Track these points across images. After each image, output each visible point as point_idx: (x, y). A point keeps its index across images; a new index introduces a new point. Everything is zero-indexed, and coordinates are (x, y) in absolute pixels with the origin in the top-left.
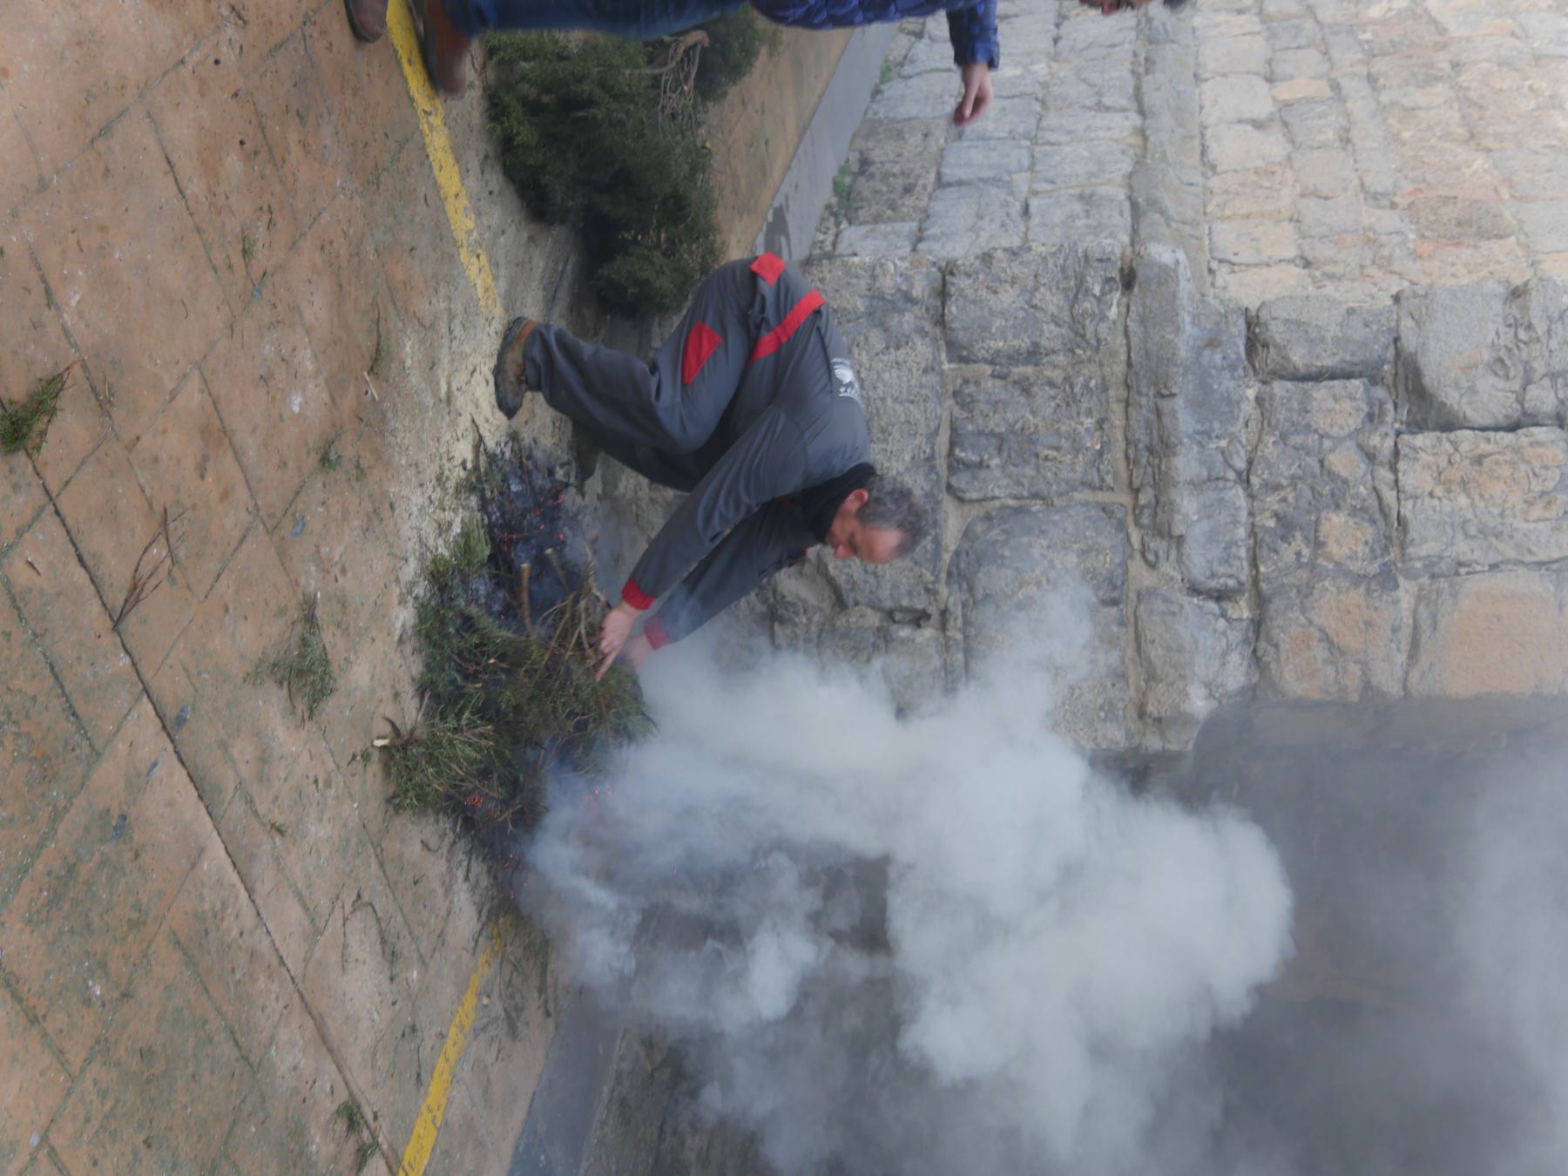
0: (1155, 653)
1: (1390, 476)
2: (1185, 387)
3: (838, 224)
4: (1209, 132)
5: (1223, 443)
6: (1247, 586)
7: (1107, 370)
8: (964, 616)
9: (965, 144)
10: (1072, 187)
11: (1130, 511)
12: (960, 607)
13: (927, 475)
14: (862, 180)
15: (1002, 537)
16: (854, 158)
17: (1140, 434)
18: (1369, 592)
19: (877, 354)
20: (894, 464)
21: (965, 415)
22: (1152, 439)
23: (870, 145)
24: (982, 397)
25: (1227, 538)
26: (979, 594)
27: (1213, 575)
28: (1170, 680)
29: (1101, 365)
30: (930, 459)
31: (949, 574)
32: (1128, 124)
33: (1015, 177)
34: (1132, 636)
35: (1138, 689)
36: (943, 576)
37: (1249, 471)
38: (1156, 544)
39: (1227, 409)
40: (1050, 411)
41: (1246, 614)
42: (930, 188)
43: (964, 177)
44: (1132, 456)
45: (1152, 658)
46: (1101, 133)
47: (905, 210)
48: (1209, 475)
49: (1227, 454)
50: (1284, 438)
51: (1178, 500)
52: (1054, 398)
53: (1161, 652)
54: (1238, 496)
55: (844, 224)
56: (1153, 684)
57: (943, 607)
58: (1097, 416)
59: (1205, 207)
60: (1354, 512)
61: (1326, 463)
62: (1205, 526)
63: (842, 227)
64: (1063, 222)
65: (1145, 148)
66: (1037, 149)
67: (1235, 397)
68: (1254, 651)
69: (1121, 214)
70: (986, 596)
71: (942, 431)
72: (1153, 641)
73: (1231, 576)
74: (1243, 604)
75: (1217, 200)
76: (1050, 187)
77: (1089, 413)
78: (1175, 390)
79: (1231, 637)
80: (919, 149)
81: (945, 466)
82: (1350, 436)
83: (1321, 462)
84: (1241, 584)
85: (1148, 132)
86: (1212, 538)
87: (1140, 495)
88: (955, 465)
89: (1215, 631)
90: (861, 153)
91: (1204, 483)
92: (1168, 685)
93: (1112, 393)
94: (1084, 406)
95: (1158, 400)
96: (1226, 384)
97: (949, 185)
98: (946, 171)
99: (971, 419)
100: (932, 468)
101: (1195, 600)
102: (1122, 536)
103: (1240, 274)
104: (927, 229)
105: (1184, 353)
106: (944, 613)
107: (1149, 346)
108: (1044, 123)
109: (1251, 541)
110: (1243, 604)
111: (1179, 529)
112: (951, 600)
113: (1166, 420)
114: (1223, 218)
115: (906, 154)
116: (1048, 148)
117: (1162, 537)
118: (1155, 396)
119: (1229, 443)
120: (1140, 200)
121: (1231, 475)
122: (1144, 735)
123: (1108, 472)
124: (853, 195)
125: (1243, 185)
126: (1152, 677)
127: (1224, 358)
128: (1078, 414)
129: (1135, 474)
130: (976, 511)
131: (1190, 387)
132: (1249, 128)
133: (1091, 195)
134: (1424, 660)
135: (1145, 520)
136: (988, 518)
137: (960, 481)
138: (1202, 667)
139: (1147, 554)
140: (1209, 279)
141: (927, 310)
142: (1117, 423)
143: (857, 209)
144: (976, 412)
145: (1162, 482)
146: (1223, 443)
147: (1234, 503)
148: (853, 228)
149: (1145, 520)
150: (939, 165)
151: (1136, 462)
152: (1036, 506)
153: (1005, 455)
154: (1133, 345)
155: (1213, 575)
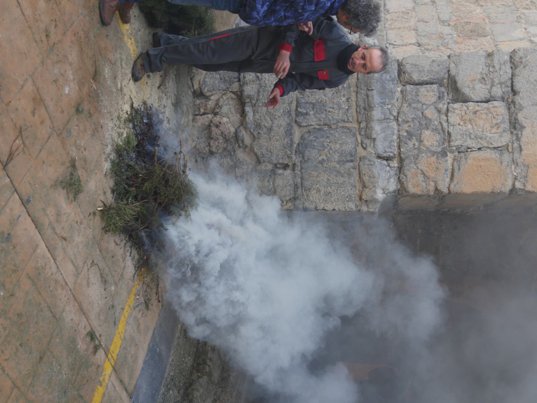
0: (366, 178)
1: (446, 118)
5: (389, 106)
6: (397, 156)
8: (301, 166)
11: (358, 130)
13: (288, 117)
18: (437, 158)
21: (301, 96)
22: (365, 105)
25: (390, 139)
26: (306, 159)
27: (385, 152)
28: (370, 188)
30: (289, 111)
31: (296, 151)
35: (359, 190)
36: (294, 152)
37: (398, 116)
38: (367, 141)
40: (330, 95)
41: (396, 165)
44: (358, 111)
48: (385, 118)
49: (391, 110)
50: (410, 105)
51: (374, 126)
53: (367, 178)
54: (394, 124)
56: (365, 189)
58: (346, 97)
59: (385, 25)
60: (433, 130)
61: (424, 113)
62: (383, 135)
68: (399, 178)
72: (365, 174)
73: (391, 152)
74: (395, 161)
75: (389, 22)
77: (344, 96)
78: (373, 88)
81: (294, 114)
82: (432, 104)
83: (422, 113)
84: (395, 155)
86: (385, 139)
87: (361, 124)
88: (298, 114)
89: (386, 171)
92: (370, 189)
93: (352, 89)
94: (342, 93)
95: (367, 91)
99: (303, 98)
100: (290, 114)
101: (379, 160)
103: (396, 49)
106: (294, 165)
109: (398, 140)
111: (374, 136)
112: (297, 160)
113: (370, 98)
114: (391, 29)
117: (368, 139)
121: (392, 118)
122: (361, 206)
123: (350, 117)
125: (398, 17)
126: (364, 186)
127: (390, 77)
129: (359, 117)
130: (305, 130)
131: (379, 87)
134: (455, 180)
135: (363, 133)
136: (309, 132)
137: (300, 119)
138: (381, 183)
139: (363, 145)
142: (353, 99)
144: (305, 95)
145: (368, 120)
146: (389, 106)
149: (363, 133)
151: (360, 113)
152: (326, 128)
155: (385, 152)
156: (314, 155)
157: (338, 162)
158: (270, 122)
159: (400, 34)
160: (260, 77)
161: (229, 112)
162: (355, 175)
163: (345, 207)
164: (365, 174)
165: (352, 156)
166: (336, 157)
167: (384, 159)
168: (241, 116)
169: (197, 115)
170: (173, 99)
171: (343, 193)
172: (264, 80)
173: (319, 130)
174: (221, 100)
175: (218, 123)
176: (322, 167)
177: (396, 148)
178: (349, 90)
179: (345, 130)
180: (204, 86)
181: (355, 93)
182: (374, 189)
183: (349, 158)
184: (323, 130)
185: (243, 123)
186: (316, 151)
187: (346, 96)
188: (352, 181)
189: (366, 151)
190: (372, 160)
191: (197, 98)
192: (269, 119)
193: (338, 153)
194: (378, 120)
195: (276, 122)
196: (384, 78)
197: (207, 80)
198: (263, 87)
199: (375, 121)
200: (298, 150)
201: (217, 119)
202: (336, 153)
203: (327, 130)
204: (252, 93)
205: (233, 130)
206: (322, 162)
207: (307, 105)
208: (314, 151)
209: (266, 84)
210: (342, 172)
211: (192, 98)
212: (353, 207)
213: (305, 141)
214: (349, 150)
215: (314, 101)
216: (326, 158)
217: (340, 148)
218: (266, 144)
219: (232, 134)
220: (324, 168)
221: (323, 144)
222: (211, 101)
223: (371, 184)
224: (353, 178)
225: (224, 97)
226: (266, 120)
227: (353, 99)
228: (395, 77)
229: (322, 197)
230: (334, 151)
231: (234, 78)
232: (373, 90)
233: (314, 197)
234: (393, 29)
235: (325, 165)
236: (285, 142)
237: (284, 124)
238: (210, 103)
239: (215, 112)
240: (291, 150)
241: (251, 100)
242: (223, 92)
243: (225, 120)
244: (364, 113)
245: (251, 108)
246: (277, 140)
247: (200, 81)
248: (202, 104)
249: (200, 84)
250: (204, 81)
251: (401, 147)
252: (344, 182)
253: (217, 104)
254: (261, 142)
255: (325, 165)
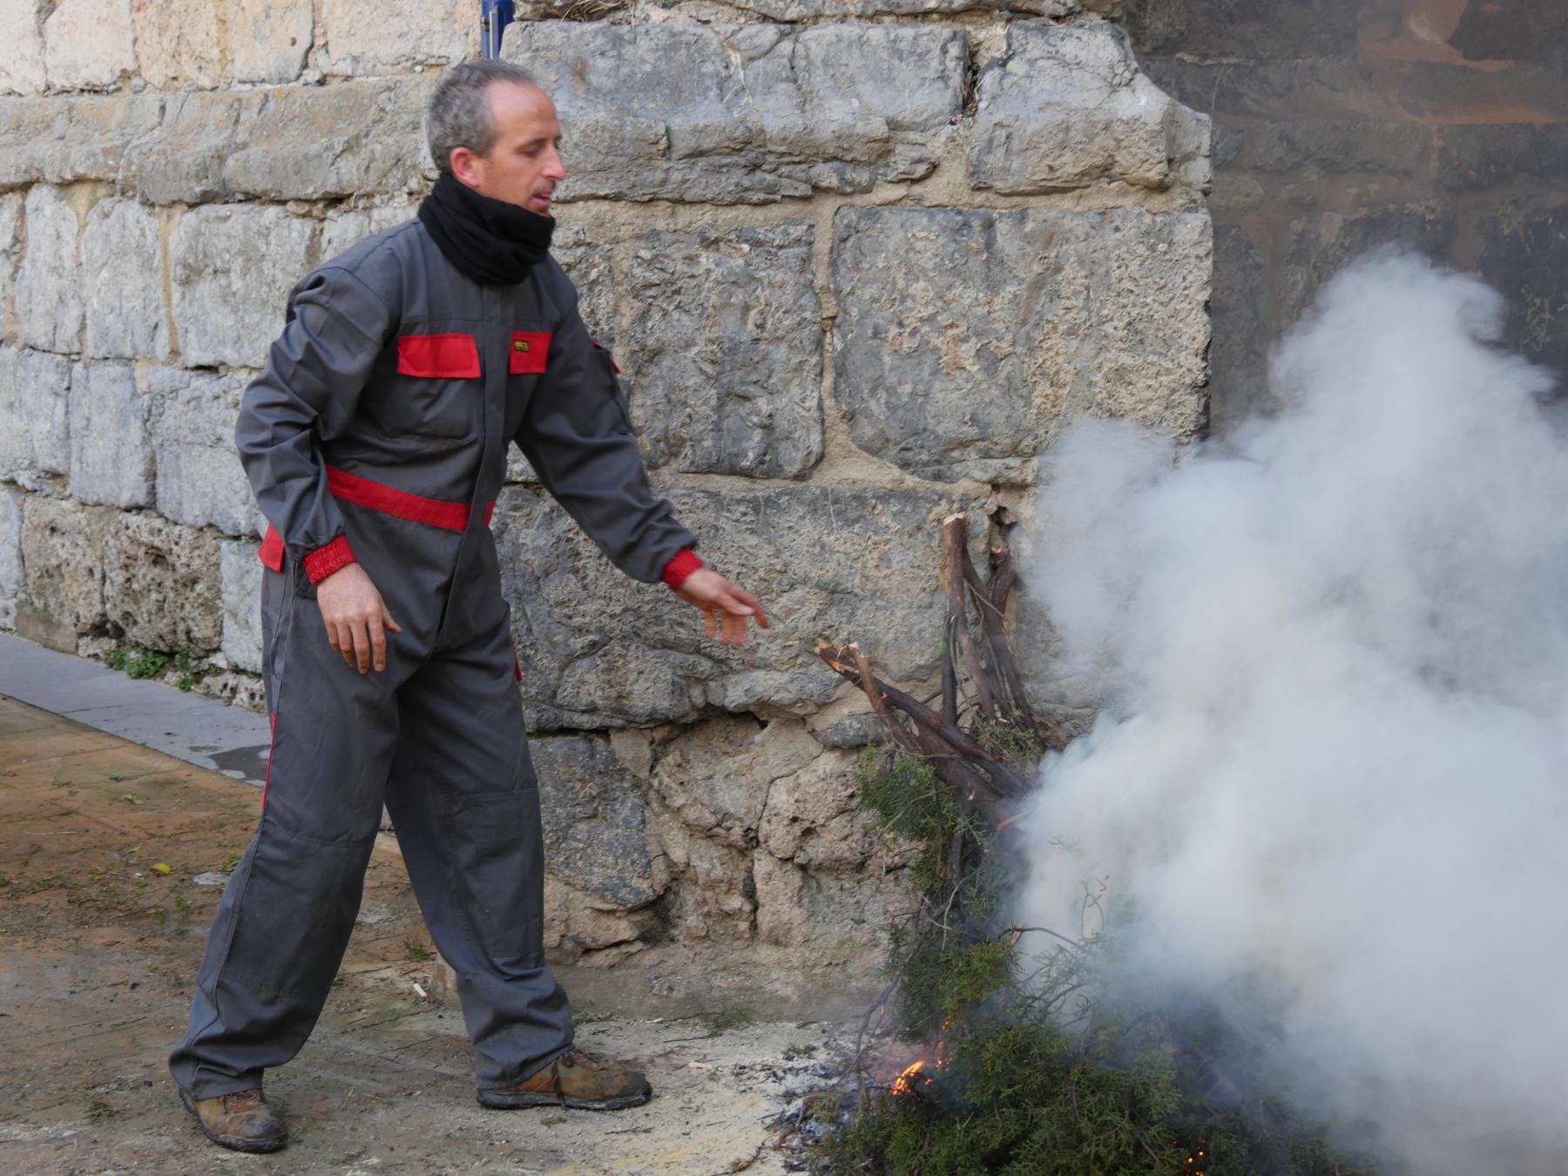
0: (1070, 165)
2: (651, 117)
3: (218, 671)
4: (59, 82)
5: (736, 58)
6: (957, 27)
7: (625, 232)
8: (1004, 455)
9: (75, 467)
10: (169, 298)
11: (848, 200)
12: (989, 461)
13: (783, 511)
14: (133, 633)
15: (883, 396)
16: (89, 646)
17: (729, 182)
19: (585, 588)
20: (760, 562)
21: (687, 450)
22: (736, 165)
23: (68, 620)
24: (659, 425)
25: (885, 55)
26: (972, 432)
27: (943, 77)
28: (1112, 144)
29: (616, 241)
30: (756, 505)
31: (937, 477)
32: (48, 210)
33: (142, 386)
34: (1041, 201)
35: (1123, 193)
36: (939, 486)
37: (776, 21)
38: (902, 159)
39: (683, 52)
40: (685, 319)
41: (999, 30)
42: (158, 523)
43: (141, 468)
44: (762, 196)
45: (1077, 171)
46: (67, 251)
47: (196, 564)
48: (787, 80)
49: (753, 53)
51: (833, 127)
52: (665, 314)
53: (1068, 157)
54: (817, 38)
55: (219, 660)
56: (1116, 170)
57: (989, 487)
58: (696, 249)
59: (201, 89)
62: (867, 89)
63: (222, 664)
64: (235, 311)
65: (98, 181)
66: (90, 351)
67: (664, 39)
68: (1057, 18)
69: (226, 219)
70: (974, 420)
71: (711, 487)
72: (1051, 168)
73: (944, 51)
74: (982, 35)
75: (189, 69)
76: (164, 332)
77: (691, 259)
78: (661, 129)
79: (1036, 53)
80: (81, 541)
81: (767, 483)
84: (954, 37)
85: (69, 176)
86: (886, 79)
87: (824, 184)
88: (767, 468)
89: (1028, 76)
90: (82, 635)
91: (799, 88)
92: (1118, 148)
93: (661, 225)
94: (681, 267)
95: (675, 155)
96: (643, 53)
97: (152, 491)
98: (125, 499)
99: (696, 441)
100: (769, 501)
101: (982, 105)
102: (886, 213)
103: (330, 36)
104: (236, 526)
105: (601, 114)
106: (996, 486)
107: (589, 167)
108: (42, 342)
109: (887, 20)
110: (982, 35)
111: (878, 128)
112: (978, 474)
113: (707, 144)
114: (225, 58)
115: (88, 563)
116: (90, 334)
117: (890, 152)
118: (669, 159)
119: (737, 49)
120: (198, 189)
121: (786, 47)
122: (1190, 185)
123: (786, 233)
124: (162, 646)
125: (162, 30)
126: (1105, 171)
127: (603, 54)
128: (693, 276)
129: (791, 192)
130: (840, 435)
131: (651, 105)
132: (53, 19)
133: (186, 266)
135: (863, 176)
136: (850, 417)
137: (793, 459)
138: (1086, 95)
139: (917, 175)
140: (334, 86)
141: (516, 508)
142: (707, 218)
143: (190, 640)
144: (684, 432)
145: (804, 152)
146: (736, 58)
147: (830, 44)
148: (225, 645)
149: (863, 176)
150: (112, 508)
151: (771, 189)
152: (834, 342)
153: (752, 389)
154: (588, 191)
155: (943, 77)
156: (956, 395)
157: (993, 287)
158: (799, 592)
159: (256, 21)
160: (591, 637)
161: (743, 780)
162: (1053, 213)
163: (1197, 257)
164: (1051, 168)
165: (966, 225)
166: (968, 296)
167: (974, 83)
168: (763, 725)
169: (754, 926)
170: (688, 1032)
171: (1134, 266)
172: (605, 620)
173: (841, 372)
174: (692, 814)
175: (797, 829)
176: (1014, 359)
177: (926, 28)
178: (669, 238)
179: (847, 256)
180: (623, 893)
181: (680, 209)
182: (1119, 129)
183: (976, 240)
184: (844, 354)
185: (793, 716)
186: (937, 385)
187: (693, 252)
188: (1079, 226)
189: (944, 165)
190: (986, 137)
191: (675, 926)
192: (784, 600)
193: (950, 287)
194: (803, 111)
195: (801, 566)
196: (608, 83)
197: (596, 881)
198: (640, 623)
199: (811, 124)
200: (931, 470)
201: (779, 836)
202: (950, 296)
203: (844, 336)
204: (666, 674)
205: (829, 763)
206: (990, 361)
207: (726, 424)
208: (940, 396)
209: (625, 610)
210: (1037, 268)
211: (672, 949)
212: (1199, 223)
213: (893, 435)
214: (941, 240)
215: (713, 392)
216: (974, 340)
217: (930, 280)
218: (899, 614)
219: (848, 765)
220: (1019, 349)
221: (909, 355)
222: (695, 861)
223: (1098, 140)
224: (1067, 223)
225: (679, 800)
226: (790, 612)
227: (707, 218)
228: (603, 32)
229: (1151, 358)
230: (940, 304)
231: (592, 756)
232: (668, 130)
233: (1148, 394)
234: (222, 51)
235: (1004, 345)
236: (895, 526)
237: (809, 530)
238: (701, 866)
239: (741, 843)
240: (927, 500)
241: (698, 680)
242: (654, 805)
243: (781, 798)
244: (770, 172)
245: (734, 678)
246: (885, 559)
247: (600, 911)
248: (705, 902)
249: (611, 912)
250: (601, 892)
251: (921, 9)
252: (1081, 262)
253: (709, 834)
254: (891, 636)
255: (1004, 345)
